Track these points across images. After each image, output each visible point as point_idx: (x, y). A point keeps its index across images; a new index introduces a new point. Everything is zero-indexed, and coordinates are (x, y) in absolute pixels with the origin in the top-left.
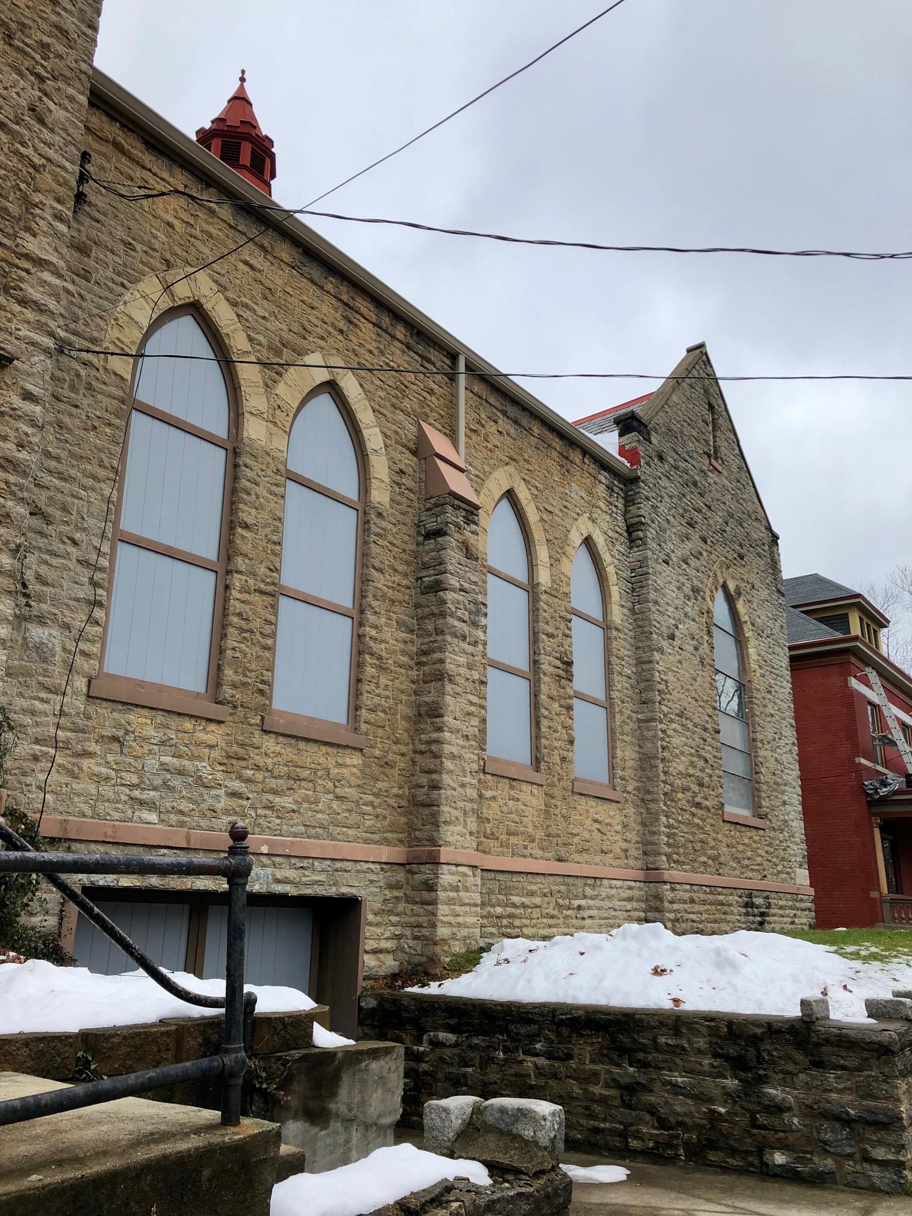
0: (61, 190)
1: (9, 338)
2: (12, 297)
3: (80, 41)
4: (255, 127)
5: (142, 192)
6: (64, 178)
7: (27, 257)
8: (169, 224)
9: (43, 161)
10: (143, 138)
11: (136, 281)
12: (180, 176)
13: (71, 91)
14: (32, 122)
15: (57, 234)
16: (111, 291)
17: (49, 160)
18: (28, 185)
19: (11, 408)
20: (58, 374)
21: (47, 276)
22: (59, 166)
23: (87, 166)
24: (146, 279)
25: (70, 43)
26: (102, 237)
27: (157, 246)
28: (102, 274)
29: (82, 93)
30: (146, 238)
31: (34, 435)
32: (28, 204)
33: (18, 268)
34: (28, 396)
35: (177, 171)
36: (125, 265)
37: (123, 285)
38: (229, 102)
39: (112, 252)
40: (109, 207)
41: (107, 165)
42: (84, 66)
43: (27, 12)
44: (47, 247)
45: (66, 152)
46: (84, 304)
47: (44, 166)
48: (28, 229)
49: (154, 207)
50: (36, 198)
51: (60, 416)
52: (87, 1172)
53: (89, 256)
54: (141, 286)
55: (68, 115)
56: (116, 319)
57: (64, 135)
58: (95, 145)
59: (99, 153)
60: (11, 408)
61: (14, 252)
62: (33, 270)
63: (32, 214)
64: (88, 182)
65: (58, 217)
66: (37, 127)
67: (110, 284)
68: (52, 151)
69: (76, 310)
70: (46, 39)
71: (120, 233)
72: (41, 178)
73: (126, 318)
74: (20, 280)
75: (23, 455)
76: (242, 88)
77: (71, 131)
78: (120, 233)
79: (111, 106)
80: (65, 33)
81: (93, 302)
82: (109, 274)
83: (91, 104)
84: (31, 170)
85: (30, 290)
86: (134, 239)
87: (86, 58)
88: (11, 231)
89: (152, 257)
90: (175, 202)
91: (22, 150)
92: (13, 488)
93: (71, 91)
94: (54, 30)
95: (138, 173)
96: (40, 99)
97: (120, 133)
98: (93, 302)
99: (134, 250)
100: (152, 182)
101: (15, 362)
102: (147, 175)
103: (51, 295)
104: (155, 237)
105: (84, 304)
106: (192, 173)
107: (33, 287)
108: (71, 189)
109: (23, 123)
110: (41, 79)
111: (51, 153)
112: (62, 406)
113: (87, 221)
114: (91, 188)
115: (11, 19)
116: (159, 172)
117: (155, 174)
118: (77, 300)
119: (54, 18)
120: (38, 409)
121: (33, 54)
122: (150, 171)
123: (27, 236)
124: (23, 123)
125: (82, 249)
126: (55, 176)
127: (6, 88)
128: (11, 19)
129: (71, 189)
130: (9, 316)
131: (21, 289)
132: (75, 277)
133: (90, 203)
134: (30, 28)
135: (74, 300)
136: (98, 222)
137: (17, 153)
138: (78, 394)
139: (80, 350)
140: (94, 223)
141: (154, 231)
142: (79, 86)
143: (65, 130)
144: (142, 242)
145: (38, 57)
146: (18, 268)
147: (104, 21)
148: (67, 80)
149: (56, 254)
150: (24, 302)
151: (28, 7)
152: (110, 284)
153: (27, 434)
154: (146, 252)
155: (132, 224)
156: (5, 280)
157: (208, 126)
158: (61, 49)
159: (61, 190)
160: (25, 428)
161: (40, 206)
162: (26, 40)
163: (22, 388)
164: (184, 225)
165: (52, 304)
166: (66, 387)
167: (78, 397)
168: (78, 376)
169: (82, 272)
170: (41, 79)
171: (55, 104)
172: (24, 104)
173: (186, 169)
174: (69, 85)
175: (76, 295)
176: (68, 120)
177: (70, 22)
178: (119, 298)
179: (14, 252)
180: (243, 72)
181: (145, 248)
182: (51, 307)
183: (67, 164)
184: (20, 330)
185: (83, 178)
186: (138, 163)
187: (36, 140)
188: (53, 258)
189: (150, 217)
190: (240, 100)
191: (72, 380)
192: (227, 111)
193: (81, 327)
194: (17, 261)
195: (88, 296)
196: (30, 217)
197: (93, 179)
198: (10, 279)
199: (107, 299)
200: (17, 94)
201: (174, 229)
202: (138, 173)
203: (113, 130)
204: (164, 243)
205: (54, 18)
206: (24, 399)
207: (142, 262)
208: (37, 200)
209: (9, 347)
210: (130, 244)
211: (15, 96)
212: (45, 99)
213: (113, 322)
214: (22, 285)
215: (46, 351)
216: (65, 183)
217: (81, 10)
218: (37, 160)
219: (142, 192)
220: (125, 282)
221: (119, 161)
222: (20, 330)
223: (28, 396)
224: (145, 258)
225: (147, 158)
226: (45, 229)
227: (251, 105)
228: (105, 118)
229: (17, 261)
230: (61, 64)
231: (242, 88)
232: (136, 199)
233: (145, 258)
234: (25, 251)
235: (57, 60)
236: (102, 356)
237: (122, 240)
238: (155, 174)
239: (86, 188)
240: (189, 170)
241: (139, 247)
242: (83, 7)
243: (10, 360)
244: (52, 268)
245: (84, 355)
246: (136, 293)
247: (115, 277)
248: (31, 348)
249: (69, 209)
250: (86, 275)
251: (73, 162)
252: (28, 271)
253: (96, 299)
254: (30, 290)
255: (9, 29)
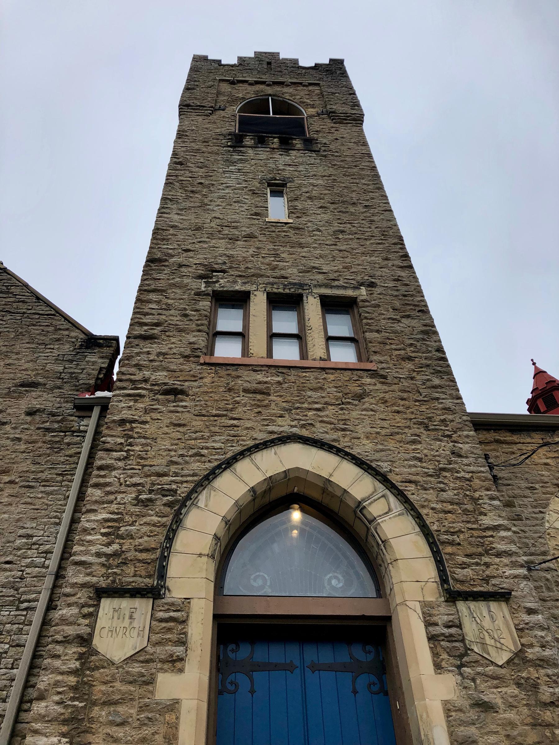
0: (486, 484)
1: (502, 580)
2: (492, 555)
3: (457, 408)
4: (555, 381)
5: (523, 457)
6: (484, 477)
7: (488, 529)
8: (546, 464)
9: (470, 474)
10: (507, 430)
11: (546, 506)
12: (537, 436)
13: (465, 433)
14: (457, 459)
15: (496, 508)
16: (537, 519)
17: (472, 472)
18: (470, 490)
19: (525, 624)
20: (536, 584)
21: (503, 533)
22: (479, 472)
23: (490, 461)
24: (551, 501)
25: (453, 412)
26: (516, 492)
27: (546, 479)
28: (527, 512)
29: (471, 431)
30: (538, 479)
31: (546, 635)
32: (475, 500)
33: (487, 537)
34: (530, 611)
35: (533, 434)
36: (536, 500)
37: (541, 512)
38: (534, 378)
39: (525, 497)
40: (510, 474)
41: (498, 454)
42: (465, 418)
43: (428, 411)
44: (495, 517)
45: (478, 463)
46: (527, 535)
47: (472, 477)
48: (481, 514)
49: (533, 460)
50: (477, 495)
51: (552, 611)
52: (475, 589)
53: (515, 506)
54: (551, 507)
55: (470, 445)
56: (549, 534)
57: (473, 456)
58: (487, 448)
59: (491, 450)
60: (525, 624)
61: (481, 530)
62: (494, 534)
63: (479, 504)
64: (494, 468)
65: (492, 498)
66: (459, 460)
67: (534, 515)
68: (472, 467)
69: (525, 540)
70: (442, 417)
71: (524, 484)
72: (474, 484)
73: (554, 530)
74: (491, 544)
75: (547, 653)
76: (536, 368)
77: (475, 451)
78: (524, 484)
79: (485, 424)
80: (448, 409)
81: (531, 531)
82: (531, 510)
83: (476, 430)
84: (468, 482)
85: (499, 546)
86: (532, 483)
87: (463, 414)
88: (473, 519)
89: (547, 487)
90: (542, 451)
91: (458, 475)
92: (554, 678)
93: (465, 433)
94: (443, 411)
95: (515, 448)
96: (454, 446)
97: (494, 434)
98: (531, 531)
99: (536, 489)
100: (524, 448)
101: (513, 593)
102: (519, 446)
103: (510, 543)
104: (543, 476)
105: (527, 535)
106: (542, 431)
107: (499, 544)
108: (490, 480)
109: (452, 462)
110: (450, 436)
111: (472, 468)
112: (549, 604)
113: (504, 488)
114: (496, 470)
115: (423, 419)
116: (525, 441)
117: (523, 443)
118: (522, 534)
119: (440, 406)
120: (540, 617)
121: (441, 428)
122: (520, 443)
123: (482, 517)
124: (452, 462)
125: (509, 504)
126: (479, 478)
127: (437, 451)
128: (423, 419)
129: (490, 480)
130: (496, 566)
131: (494, 548)
132: (514, 522)
133: (500, 477)
134: (433, 417)
135: (520, 535)
136: (509, 485)
137: (457, 478)
138: (554, 591)
139: (540, 564)
140: (508, 487)
141: (540, 473)
142: (468, 428)
143: (472, 453)
144: (538, 482)
145: (443, 428)
146: (487, 537)
147: (462, 393)
148: (460, 429)
149: (501, 519)
150: (499, 555)
151: (427, 409)
152: (534, 515)
153: (542, 637)
154: (542, 487)
155: (526, 476)
156: (484, 548)
157: (530, 396)
158: (450, 417)
159: (486, 484)
160: (540, 633)
161: (480, 498)
162: (435, 423)
163: (525, 608)
164: (554, 459)
165: (513, 548)
166: (544, 590)
167: (555, 594)
168: (547, 580)
169: (516, 517)
170: (450, 436)
171: (462, 443)
172: (448, 453)
173: (537, 431)
174: (463, 431)
175: (520, 532)
176: (471, 447)
177: (449, 403)
178: (543, 521)
179: (481, 530)
180: (532, 360)
181: (541, 485)
182: (513, 549)
183: (482, 469)
184: (505, 572)
185: (491, 468)
186: (512, 443)
187: (462, 467)
188: (501, 522)
189: (533, 466)
190: (539, 374)
191: (545, 584)
192: (536, 383)
193: (533, 549)
194: (484, 534)
195: (526, 529)
196: (479, 506)
197: (495, 466)
198: (486, 546)
199: (537, 525)
200: (443, 450)
201: (550, 465)
202: (515, 448)
203: (491, 436)
204: (549, 476)
205: (440, 406)
206: (529, 615)
207: (544, 493)
208: (478, 496)
209: (504, 585)
210: (532, 487)
211: (443, 452)
212: (456, 444)
213: (547, 536)
214: (493, 546)
215: (525, 578)
216: (486, 479)
217: (450, 394)
218: (468, 476)
219: (523, 457)
220: (541, 510)
221: (503, 448)
222: (505, 572)
223: (530, 611)
224: (544, 490)
225: (515, 438)
226: (489, 508)
227: (545, 372)
228: (485, 432)
229: (484, 534)
230: (454, 424)
231: (536, 368)
232: (521, 463)
233: (544, 490)
234: (486, 526)
235: (452, 424)
236: (554, 561)
237: (526, 488)
238: (523, 443)
239: (495, 472)
240: (539, 430)
241: (537, 486)
242: (450, 392)
243: (510, 594)
244: (503, 527)
245: (543, 565)
246: (551, 512)
247: (535, 510)
248: (516, 580)
249: (494, 491)
250: (519, 518)
251: (484, 466)
252: (492, 536)
253: (531, 528)
254: (499, 546)
255: (425, 424)
